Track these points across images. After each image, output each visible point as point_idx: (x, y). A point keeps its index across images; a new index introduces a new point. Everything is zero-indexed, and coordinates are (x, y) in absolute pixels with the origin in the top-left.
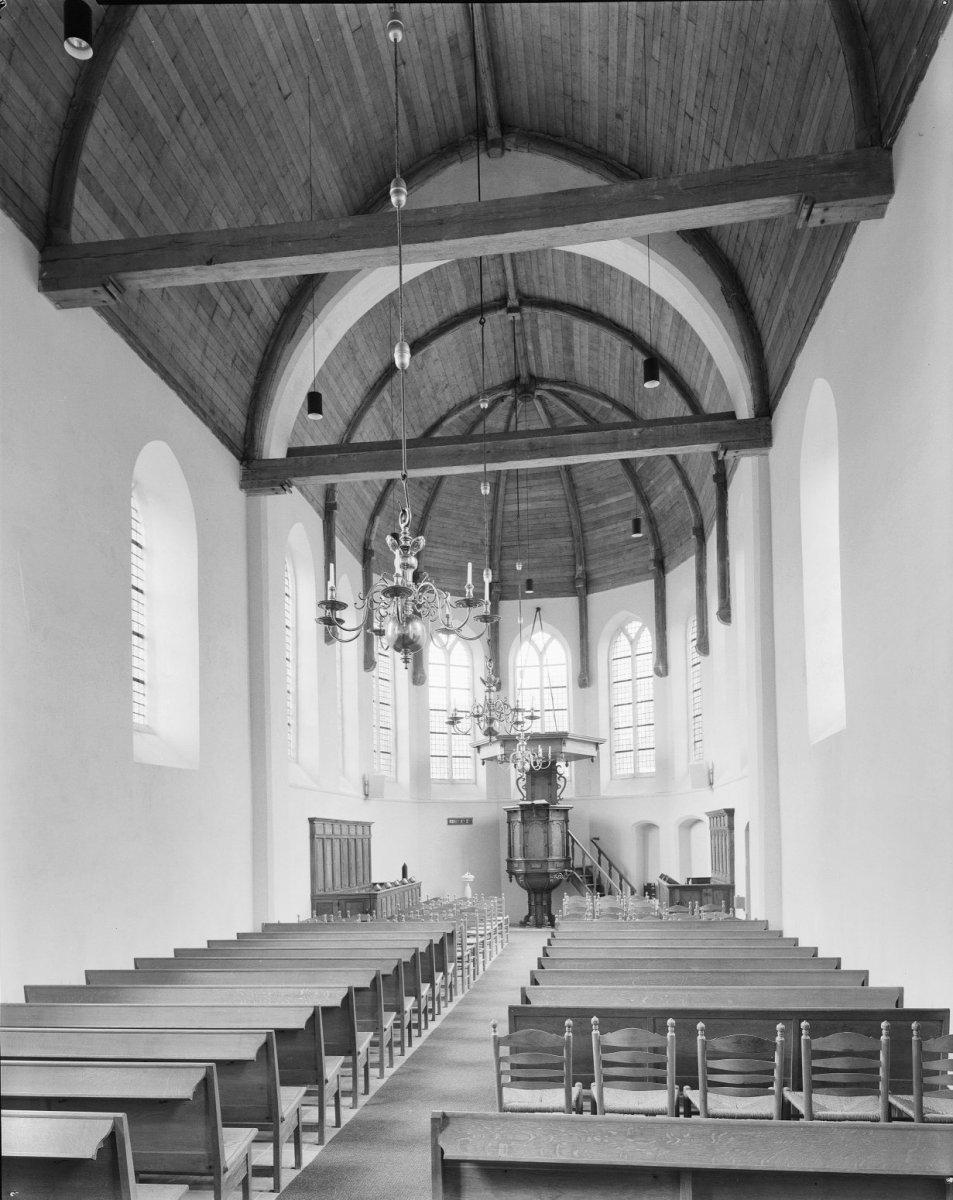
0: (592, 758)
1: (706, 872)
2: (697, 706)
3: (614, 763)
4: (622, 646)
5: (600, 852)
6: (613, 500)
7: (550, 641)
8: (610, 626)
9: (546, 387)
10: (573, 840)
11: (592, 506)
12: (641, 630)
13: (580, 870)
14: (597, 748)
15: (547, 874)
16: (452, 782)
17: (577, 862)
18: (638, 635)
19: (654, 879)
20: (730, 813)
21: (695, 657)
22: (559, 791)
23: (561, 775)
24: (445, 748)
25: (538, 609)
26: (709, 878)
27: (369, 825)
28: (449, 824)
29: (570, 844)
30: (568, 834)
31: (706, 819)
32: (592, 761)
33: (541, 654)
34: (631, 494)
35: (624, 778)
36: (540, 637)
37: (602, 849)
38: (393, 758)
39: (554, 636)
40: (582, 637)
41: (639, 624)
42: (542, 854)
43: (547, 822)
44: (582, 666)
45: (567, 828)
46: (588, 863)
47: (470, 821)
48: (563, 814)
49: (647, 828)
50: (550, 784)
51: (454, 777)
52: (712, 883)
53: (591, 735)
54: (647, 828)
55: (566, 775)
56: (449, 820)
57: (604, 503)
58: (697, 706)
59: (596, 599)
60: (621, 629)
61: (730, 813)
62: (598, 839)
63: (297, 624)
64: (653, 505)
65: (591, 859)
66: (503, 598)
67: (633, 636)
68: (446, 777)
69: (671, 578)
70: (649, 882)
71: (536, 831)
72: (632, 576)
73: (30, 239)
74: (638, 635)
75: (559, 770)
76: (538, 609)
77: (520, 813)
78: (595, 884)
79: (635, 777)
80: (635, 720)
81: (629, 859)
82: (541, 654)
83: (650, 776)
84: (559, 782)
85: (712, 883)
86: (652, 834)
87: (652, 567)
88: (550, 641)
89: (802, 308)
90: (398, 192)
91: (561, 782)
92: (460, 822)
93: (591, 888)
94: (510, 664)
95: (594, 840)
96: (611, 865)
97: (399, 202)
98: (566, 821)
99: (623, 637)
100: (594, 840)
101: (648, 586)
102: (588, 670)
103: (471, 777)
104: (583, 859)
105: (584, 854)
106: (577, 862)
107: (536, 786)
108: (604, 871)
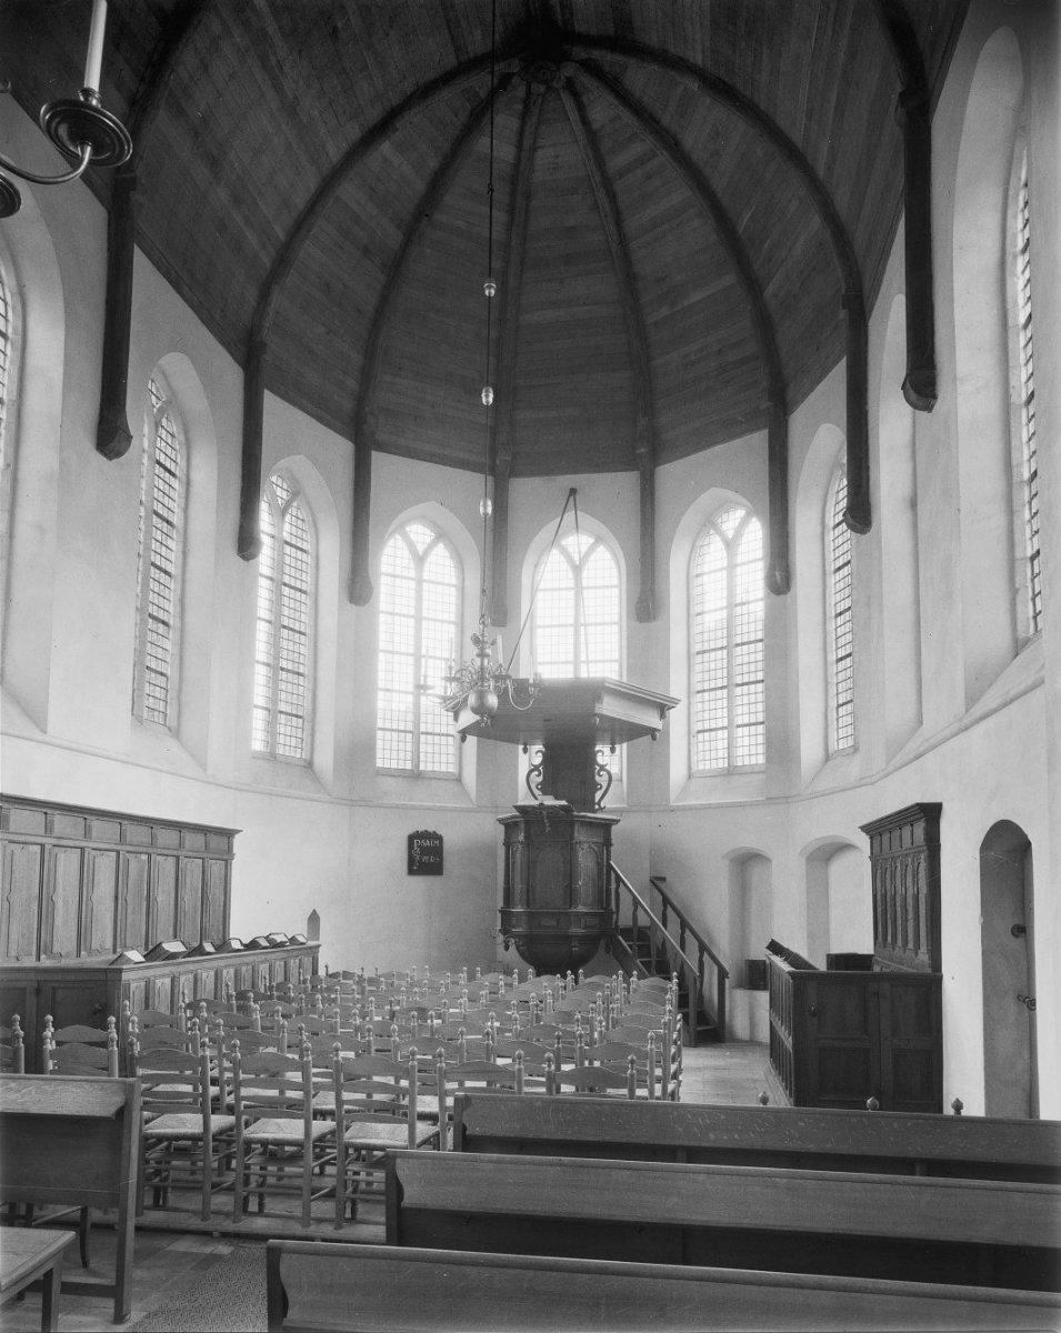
0: (652, 732)
1: (862, 943)
2: (842, 641)
3: (694, 749)
4: (714, 551)
5: (666, 901)
6: (696, 296)
7: (592, 549)
8: (690, 518)
9: (580, 53)
10: (619, 879)
11: (665, 311)
12: (744, 522)
13: (627, 932)
14: (662, 716)
15: (568, 938)
16: (416, 776)
17: (625, 919)
19: (759, 952)
20: (929, 814)
21: (842, 539)
22: (598, 795)
23: (602, 768)
24: (452, 759)
25: (573, 492)
26: (869, 957)
27: (228, 834)
29: (613, 886)
30: (610, 868)
31: (863, 841)
32: (654, 738)
33: (577, 570)
34: (730, 279)
36: (577, 542)
37: (671, 896)
38: (307, 726)
39: (599, 539)
41: (740, 513)
45: (609, 859)
46: (643, 921)
49: (746, 863)
52: (877, 969)
53: (653, 688)
54: (746, 863)
55: (614, 770)
57: (686, 303)
58: (842, 641)
59: (670, 474)
60: (709, 523)
61: (929, 814)
63: (316, 630)
64: (769, 291)
65: (649, 914)
67: (730, 534)
69: (798, 420)
72: (729, 429)
75: (600, 759)
76: (573, 492)
77: (523, 826)
78: (654, 959)
79: (731, 771)
80: (730, 677)
81: (714, 910)
82: (577, 570)
83: (751, 771)
85: (877, 969)
86: (756, 873)
87: (765, 404)
88: (592, 549)
90: (490, 287)
91: (602, 780)
93: (647, 965)
94: (526, 581)
96: (684, 925)
97: (490, 293)
98: (607, 843)
100: (657, 882)
101: (759, 440)
102: (652, 591)
105: (636, 903)
106: (625, 919)
108: (671, 935)
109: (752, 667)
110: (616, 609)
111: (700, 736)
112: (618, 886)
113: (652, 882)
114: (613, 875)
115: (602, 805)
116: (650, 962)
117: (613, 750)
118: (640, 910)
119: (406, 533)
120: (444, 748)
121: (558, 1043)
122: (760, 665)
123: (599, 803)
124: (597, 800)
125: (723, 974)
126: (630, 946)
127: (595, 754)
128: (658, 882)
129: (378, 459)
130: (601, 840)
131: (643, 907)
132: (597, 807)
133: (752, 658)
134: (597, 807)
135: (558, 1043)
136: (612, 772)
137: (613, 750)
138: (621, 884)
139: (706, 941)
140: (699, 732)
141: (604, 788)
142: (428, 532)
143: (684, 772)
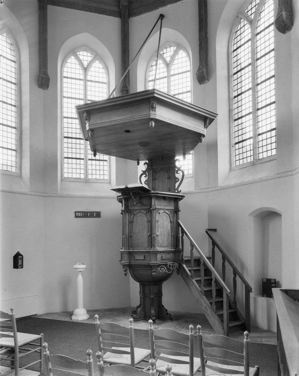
5: (214, 244)
10: (183, 231)
13: (188, 262)
16: (86, 181)
18: (90, 64)
23: (179, 169)
28: (76, 217)
29: (181, 235)
30: (179, 225)
35: (243, 167)
40: (200, 30)
42: (146, 245)
43: (150, 211)
44: (201, 59)
46: (196, 255)
47: (98, 215)
48: (172, 203)
50: (169, 178)
51: (90, 177)
56: (76, 212)
62: (215, 230)
66: (131, 14)
68: (82, 176)
70: (269, 277)
71: (141, 220)
73: (47, 54)
74: (90, 64)
75: (177, 164)
79: (256, 163)
83: (270, 159)
84: (177, 175)
86: (272, 224)
89: (220, 292)
91: (179, 176)
92: (86, 215)
95: (210, 231)
98: (176, 211)
99: (244, 22)
103: (106, 177)
104: (192, 250)
105: (192, 245)
106: (186, 254)
107: (157, 181)
109: (269, 147)
110: (189, 84)
111: (237, 145)
112: (183, 236)
113: (207, 232)
114: (180, 228)
115: (179, 190)
116: (200, 280)
117: (184, 158)
118: (194, 250)
119: (77, 55)
120: (94, 167)
121: (151, 326)
122: (274, 146)
123: (177, 190)
124: (176, 187)
125: (248, 290)
126: (190, 270)
127: (175, 161)
128: (212, 234)
129: (51, 9)
130: (172, 208)
131: (197, 249)
132: (176, 191)
133: (269, 141)
134: (176, 191)
135: (151, 326)
136: (186, 173)
137: (184, 158)
138: (185, 234)
139: (239, 269)
140: (236, 144)
141: (180, 180)
142: (89, 54)
143: (227, 166)
